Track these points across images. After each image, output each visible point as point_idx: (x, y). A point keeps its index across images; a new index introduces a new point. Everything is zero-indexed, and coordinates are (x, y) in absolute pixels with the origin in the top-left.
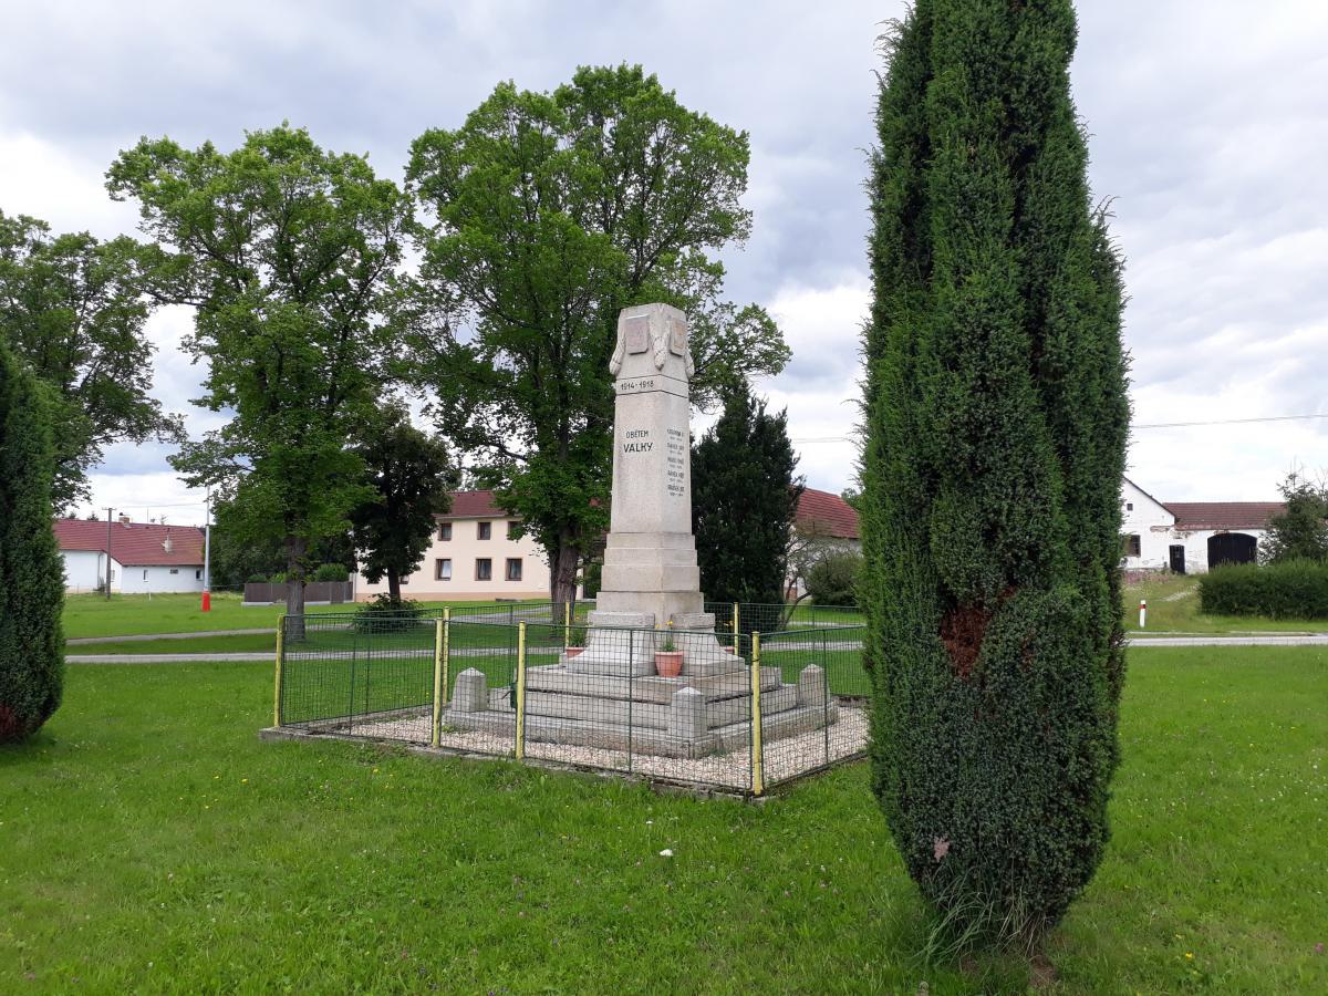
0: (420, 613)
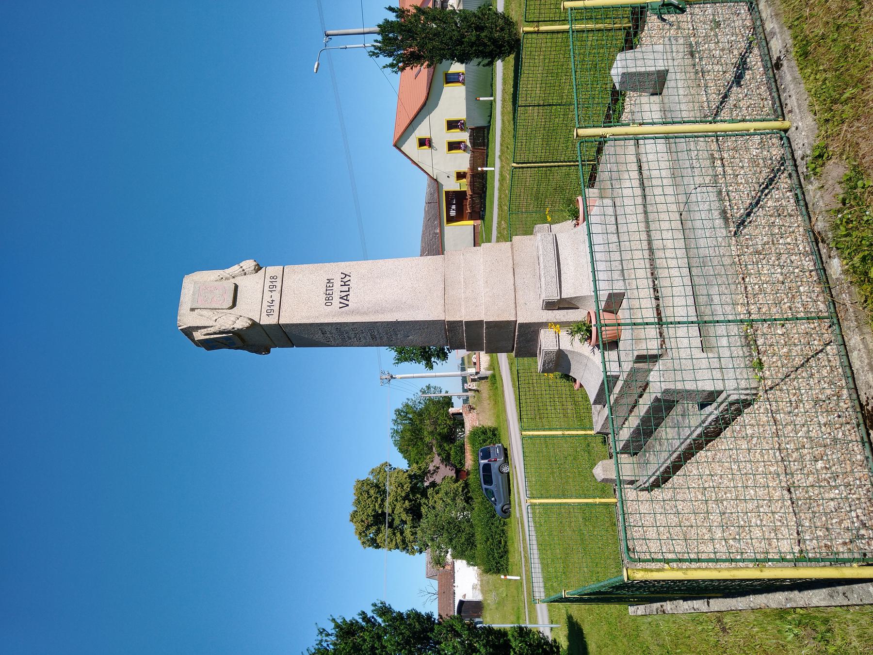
0: (392, 65)
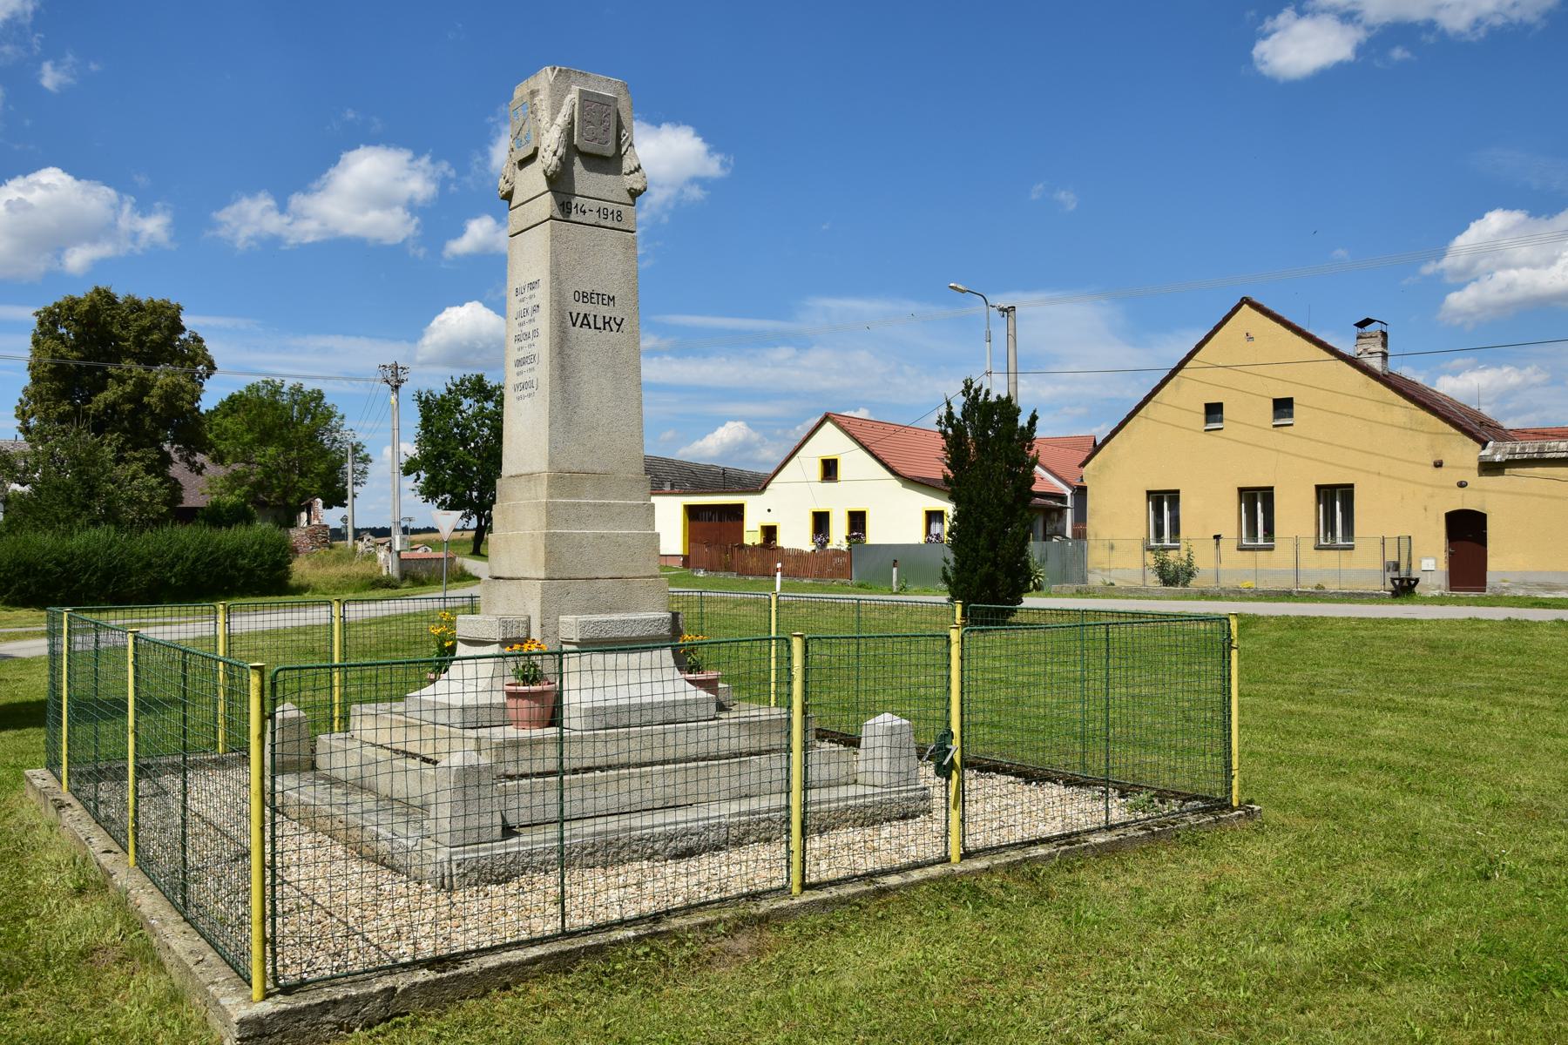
0: (950, 415)
